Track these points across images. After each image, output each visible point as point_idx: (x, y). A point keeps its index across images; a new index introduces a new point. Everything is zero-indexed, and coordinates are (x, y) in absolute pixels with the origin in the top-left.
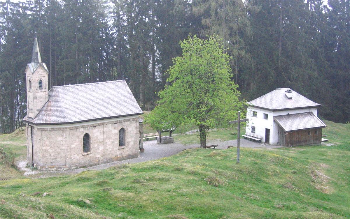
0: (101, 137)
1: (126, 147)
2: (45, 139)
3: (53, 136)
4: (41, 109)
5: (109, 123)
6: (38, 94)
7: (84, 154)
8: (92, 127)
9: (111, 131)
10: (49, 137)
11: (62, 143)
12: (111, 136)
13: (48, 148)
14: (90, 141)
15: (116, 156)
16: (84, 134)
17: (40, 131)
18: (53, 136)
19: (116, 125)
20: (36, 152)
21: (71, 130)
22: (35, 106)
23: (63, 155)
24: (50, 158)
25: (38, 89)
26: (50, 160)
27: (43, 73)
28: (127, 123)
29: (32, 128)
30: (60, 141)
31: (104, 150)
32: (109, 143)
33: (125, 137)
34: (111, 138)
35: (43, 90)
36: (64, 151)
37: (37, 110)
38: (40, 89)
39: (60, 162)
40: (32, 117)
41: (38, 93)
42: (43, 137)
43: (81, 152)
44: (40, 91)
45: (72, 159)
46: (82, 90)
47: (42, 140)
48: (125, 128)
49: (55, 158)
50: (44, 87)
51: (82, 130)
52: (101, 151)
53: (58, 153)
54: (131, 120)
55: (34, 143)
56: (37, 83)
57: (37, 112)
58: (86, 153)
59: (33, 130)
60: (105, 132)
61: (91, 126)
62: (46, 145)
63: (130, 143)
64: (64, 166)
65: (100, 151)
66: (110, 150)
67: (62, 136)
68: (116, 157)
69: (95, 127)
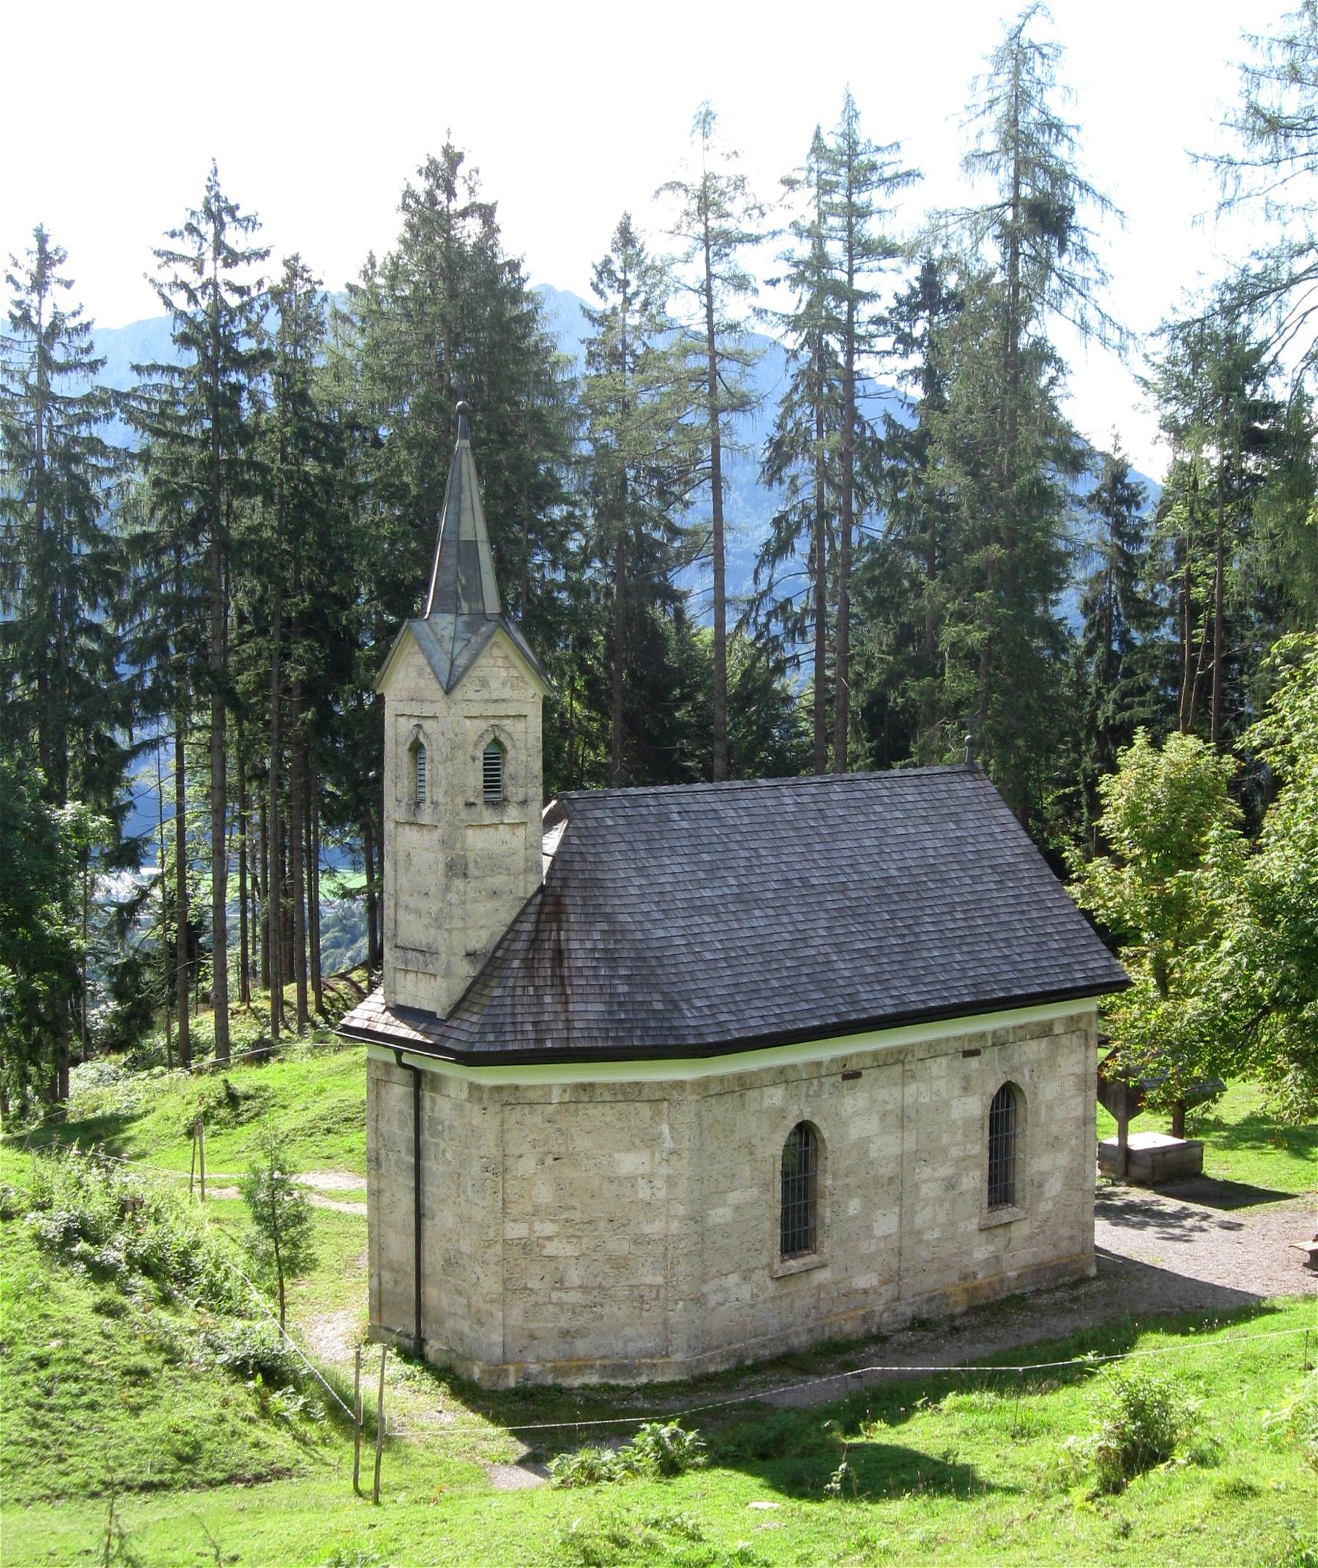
0: (886, 1147)
1: (1022, 1214)
2: (528, 1165)
3: (583, 1143)
4: (496, 950)
5: (934, 1051)
6: (476, 841)
7: (780, 1269)
8: (839, 1078)
9: (947, 1104)
10: (555, 1149)
11: (643, 1193)
12: (945, 1139)
13: (548, 1228)
14: (820, 1179)
15: (964, 1278)
16: (791, 1123)
17: (494, 1108)
18: (583, 1143)
19: (974, 1063)
20: (448, 1261)
21: (713, 1101)
22: (458, 924)
23: (649, 1280)
24: (560, 1304)
25: (480, 801)
26: (556, 1317)
27: (516, 695)
28: (1034, 1049)
29: (417, 1086)
30: (632, 1180)
31: (901, 1238)
32: (929, 1190)
33: (1019, 1143)
34: (945, 1151)
35: (513, 814)
36: (662, 1249)
37: (470, 955)
38: (489, 803)
39: (629, 1332)
40: (427, 1007)
41: (477, 831)
42: (513, 1150)
43: (764, 1259)
44: (489, 816)
45: (712, 1304)
46: (746, 820)
47: (505, 1171)
48: (1023, 1079)
49: (589, 1299)
50: (514, 791)
51: (775, 1096)
52: (882, 1245)
53: (620, 1264)
54: (1058, 1029)
55: (432, 1190)
56: (474, 759)
57: (466, 971)
58: (794, 1264)
59: (427, 1096)
60: (912, 1113)
61: (834, 1069)
62: (530, 1209)
63: (1047, 1186)
64: (652, 1357)
65: (873, 1249)
66: (936, 1234)
67: (651, 1142)
68: (969, 1284)
69: (856, 1075)
